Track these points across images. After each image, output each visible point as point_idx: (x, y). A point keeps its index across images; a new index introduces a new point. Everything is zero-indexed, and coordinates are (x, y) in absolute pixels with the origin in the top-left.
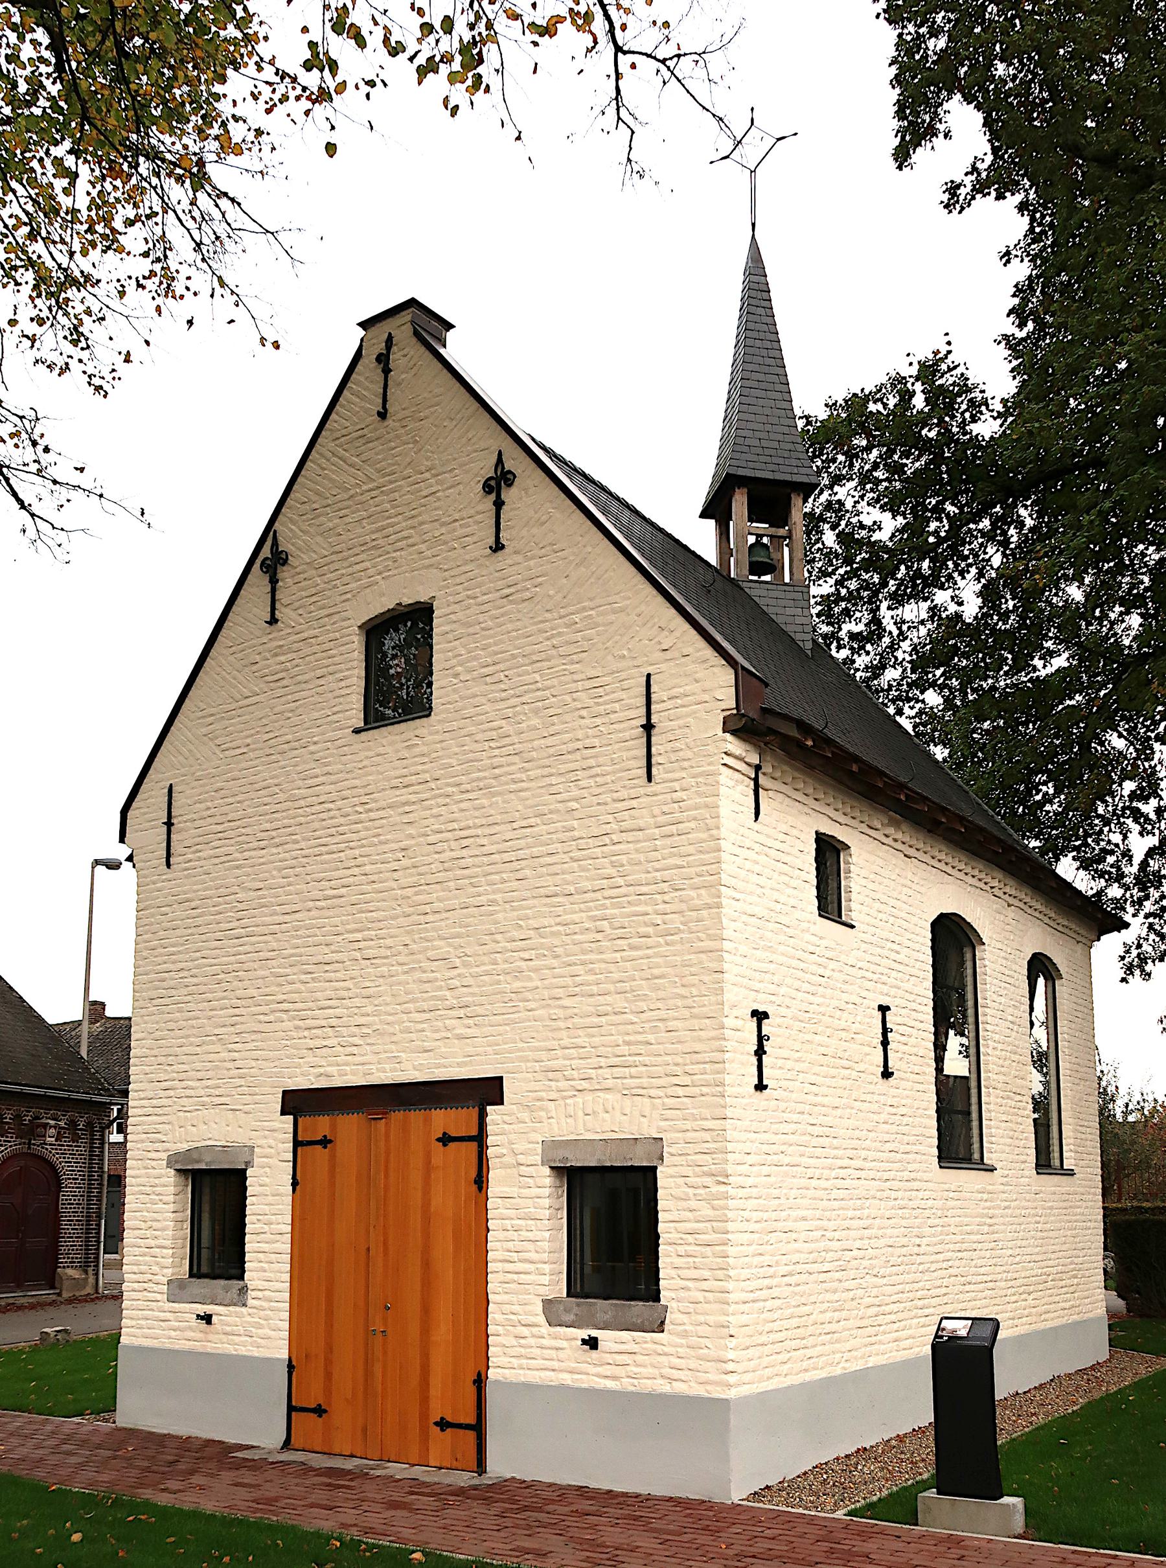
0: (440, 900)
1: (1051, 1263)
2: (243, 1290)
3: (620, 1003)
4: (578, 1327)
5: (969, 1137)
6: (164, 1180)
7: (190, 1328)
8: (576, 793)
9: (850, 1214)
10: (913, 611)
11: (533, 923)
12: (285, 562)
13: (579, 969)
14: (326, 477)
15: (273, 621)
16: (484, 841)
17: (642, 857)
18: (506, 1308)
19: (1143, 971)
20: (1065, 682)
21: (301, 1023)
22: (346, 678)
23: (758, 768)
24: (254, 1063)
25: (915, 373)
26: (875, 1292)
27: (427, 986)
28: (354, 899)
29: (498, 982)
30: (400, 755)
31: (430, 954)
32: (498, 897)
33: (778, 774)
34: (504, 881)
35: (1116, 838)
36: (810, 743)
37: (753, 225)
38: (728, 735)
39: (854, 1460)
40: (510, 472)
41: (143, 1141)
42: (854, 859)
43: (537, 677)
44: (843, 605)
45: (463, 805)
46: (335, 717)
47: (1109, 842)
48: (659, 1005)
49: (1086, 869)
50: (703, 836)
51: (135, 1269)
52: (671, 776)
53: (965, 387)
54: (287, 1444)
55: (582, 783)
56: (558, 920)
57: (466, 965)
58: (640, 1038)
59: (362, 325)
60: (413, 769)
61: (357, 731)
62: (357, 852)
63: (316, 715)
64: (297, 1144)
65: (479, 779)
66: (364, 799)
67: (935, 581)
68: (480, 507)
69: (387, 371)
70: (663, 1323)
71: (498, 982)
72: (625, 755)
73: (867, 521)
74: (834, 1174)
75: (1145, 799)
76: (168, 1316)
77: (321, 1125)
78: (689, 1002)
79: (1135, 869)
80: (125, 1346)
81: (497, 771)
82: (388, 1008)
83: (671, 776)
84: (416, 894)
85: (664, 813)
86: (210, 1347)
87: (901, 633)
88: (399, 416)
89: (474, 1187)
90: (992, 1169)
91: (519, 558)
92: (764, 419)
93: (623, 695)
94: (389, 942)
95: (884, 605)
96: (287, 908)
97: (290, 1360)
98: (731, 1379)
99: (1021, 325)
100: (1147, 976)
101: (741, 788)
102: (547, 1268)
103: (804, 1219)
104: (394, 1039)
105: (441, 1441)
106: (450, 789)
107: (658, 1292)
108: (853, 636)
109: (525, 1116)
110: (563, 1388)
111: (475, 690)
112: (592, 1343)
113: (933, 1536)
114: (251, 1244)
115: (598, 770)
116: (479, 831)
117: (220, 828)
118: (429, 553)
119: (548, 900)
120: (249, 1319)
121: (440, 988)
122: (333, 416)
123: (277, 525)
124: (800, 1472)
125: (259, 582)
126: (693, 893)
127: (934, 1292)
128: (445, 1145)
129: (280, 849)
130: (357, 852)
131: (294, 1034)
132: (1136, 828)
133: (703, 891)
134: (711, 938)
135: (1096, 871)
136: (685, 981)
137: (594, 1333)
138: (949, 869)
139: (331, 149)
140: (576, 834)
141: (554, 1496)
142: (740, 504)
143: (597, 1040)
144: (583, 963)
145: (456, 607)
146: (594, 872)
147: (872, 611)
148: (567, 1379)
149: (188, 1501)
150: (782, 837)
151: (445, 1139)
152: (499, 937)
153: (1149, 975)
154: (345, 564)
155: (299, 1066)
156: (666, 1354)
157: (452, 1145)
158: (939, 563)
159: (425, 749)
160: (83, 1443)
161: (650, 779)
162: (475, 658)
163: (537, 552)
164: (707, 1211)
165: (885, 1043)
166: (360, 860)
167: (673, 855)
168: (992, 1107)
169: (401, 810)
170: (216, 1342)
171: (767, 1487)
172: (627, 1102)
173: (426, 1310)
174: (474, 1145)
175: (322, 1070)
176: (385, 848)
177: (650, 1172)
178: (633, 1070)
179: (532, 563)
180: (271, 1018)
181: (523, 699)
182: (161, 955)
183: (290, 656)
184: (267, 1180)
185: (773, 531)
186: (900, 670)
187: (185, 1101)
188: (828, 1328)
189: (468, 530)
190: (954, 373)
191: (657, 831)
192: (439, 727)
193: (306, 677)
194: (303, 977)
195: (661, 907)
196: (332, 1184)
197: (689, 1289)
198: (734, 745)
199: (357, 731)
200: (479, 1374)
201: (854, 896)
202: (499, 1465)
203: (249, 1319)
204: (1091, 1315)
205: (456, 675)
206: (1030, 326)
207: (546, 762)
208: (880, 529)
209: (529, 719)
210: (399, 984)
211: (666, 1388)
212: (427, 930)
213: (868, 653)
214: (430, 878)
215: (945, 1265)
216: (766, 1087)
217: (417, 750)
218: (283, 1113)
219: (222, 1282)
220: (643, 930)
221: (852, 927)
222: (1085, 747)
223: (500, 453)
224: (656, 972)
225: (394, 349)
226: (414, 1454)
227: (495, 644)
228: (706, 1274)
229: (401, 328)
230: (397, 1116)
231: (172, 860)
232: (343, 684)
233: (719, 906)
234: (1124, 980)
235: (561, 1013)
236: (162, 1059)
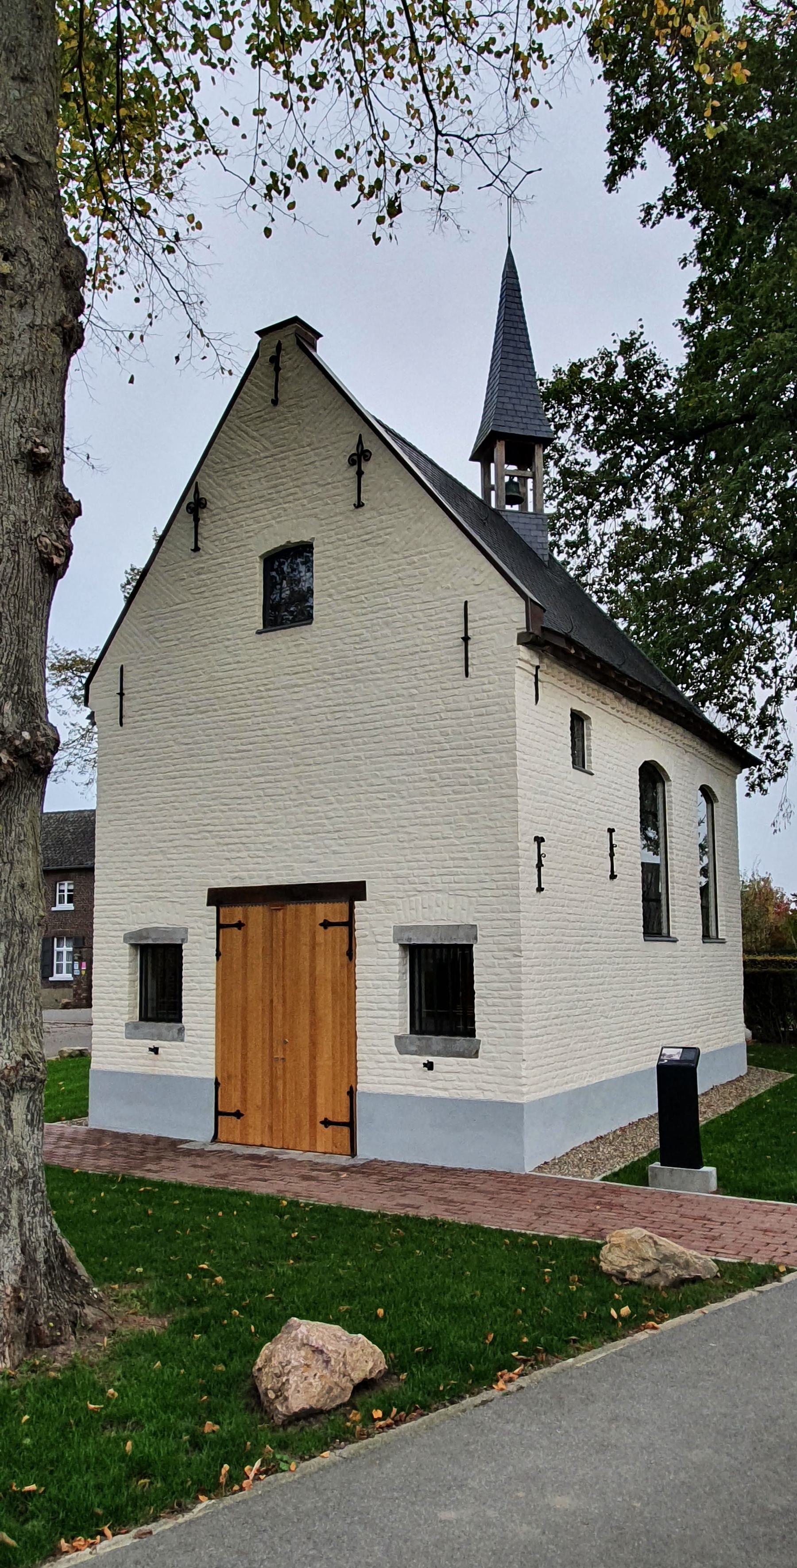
0: (320, 755)
1: (711, 1006)
2: (181, 1031)
3: (447, 830)
4: (420, 1055)
5: (660, 918)
6: (122, 951)
7: (143, 1057)
8: (416, 683)
9: (592, 974)
10: (612, 525)
11: (387, 773)
12: (205, 506)
13: (418, 807)
14: (233, 445)
15: (196, 549)
16: (351, 715)
17: (462, 730)
18: (370, 1042)
19: (761, 788)
20: (713, 574)
21: (221, 841)
22: (251, 593)
23: (537, 668)
24: (187, 869)
25: (618, 349)
26: (606, 1028)
27: (311, 816)
28: (259, 752)
29: (362, 815)
30: (290, 651)
31: (314, 793)
32: (361, 754)
33: (550, 671)
34: (365, 743)
35: (745, 689)
36: (573, 651)
37: (509, 238)
38: (521, 647)
39: (596, 1145)
40: (368, 451)
41: (105, 923)
42: (593, 727)
43: (388, 599)
44: (562, 520)
45: (337, 689)
46: (242, 622)
47: (740, 693)
48: (474, 833)
49: (723, 712)
50: (504, 716)
51: (101, 1015)
52: (482, 673)
53: (652, 361)
54: (215, 1139)
55: (420, 676)
56: (404, 772)
57: (339, 802)
58: (461, 855)
59: (258, 333)
60: (300, 662)
61: (259, 633)
62: (260, 719)
63: (230, 619)
64: (220, 926)
65: (347, 670)
66: (265, 681)
67: (625, 503)
68: (346, 475)
69: (277, 369)
70: (477, 1052)
71: (362, 815)
72: (449, 657)
73: (581, 460)
74: (582, 947)
75: (765, 661)
76: (127, 1049)
77: (237, 913)
78: (494, 831)
79: (757, 712)
80: (97, 1071)
81: (360, 665)
82: (283, 831)
83: (482, 673)
84: (303, 750)
85: (477, 700)
86: (157, 1071)
87: (603, 543)
88: (287, 404)
89: (346, 958)
90: (675, 941)
91: (375, 513)
92: (516, 389)
93: (448, 615)
94: (284, 784)
95: (592, 520)
96: (210, 758)
97: (216, 1079)
98: (525, 1089)
99: (691, 312)
100: (764, 792)
101: (527, 682)
102: (397, 1014)
103: (565, 979)
104: (289, 853)
105: (325, 1135)
106: (327, 677)
107: (474, 1030)
108: (567, 543)
109: (381, 908)
110: (409, 1097)
111: (344, 607)
112: (429, 1066)
113: (660, 1193)
114: (186, 998)
115: (431, 668)
116: (347, 708)
117: (159, 698)
118: (309, 506)
119: (396, 758)
120: (185, 1050)
121: (320, 818)
122: (238, 400)
123: (197, 479)
124: (563, 1153)
125: (186, 519)
126: (497, 756)
127: (640, 1028)
128: (325, 928)
129: (203, 715)
130: (260, 719)
131: (215, 848)
132: (759, 682)
133: (503, 754)
134: (509, 787)
135: (730, 714)
136: (491, 817)
137: (431, 1059)
138: (649, 729)
139: (268, 232)
140: (416, 711)
141: (407, 1170)
142: (500, 451)
143: (431, 857)
144: (422, 802)
145: (330, 547)
146: (428, 739)
147: (581, 525)
148: (412, 1090)
149: (169, 1177)
150: (551, 714)
151: (326, 924)
152: (362, 782)
153: (766, 791)
154: (249, 510)
155: (220, 871)
156: (480, 1073)
157: (331, 929)
158: (628, 490)
159: (308, 647)
160: (74, 1140)
161: (467, 675)
162: (345, 584)
163: (387, 510)
164: (508, 976)
165: (612, 855)
166: (262, 726)
167: (483, 729)
168: (675, 896)
169: (291, 690)
170: (161, 1067)
171: (546, 1163)
172: (452, 900)
173: (313, 1043)
174: (345, 930)
175: (236, 874)
176: (280, 717)
177: (467, 949)
178: (456, 878)
179: (383, 517)
180: (199, 836)
181: (378, 615)
182: (117, 789)
183: (210, 575)
184: (198, 952)
185: (521, 473)
186: (601, 570)
187: (136, 895)
188: (579, 1054)
189: (337, 491)
190: (644, 349)
191: (472, 711)
192: (318, 632)
193: (221, 592)
194: (222, 807)
195: (475, 765)
196: (245, 956)
197: (495, 1028)
198: (524, 652)
199: (259, 633)
200: (351, 1088)
201: (593, 752)
202: (365, 1152)
203: (185, 1050)
204: (735, 1042)
205: (330, 596)
206: (698, 312)
207: (395, 660)
208: (589, 464)
209: (382, 629)
210: (292, 814)
211: (481, 1097)
212: (310, 776)
213: (579, 557)
214: (312, 740)
215: (647, 1009)
216: (542, 889)
217: (302, 648)
218: (209, 904)
219: (166, 1024)
220: (462, 780)
221: (592, 774)
222: (726, 623)
223: (360, 436)
224: (472, 810)
225: (283, 353)
226: (306, 1145)
227: (358, 575)
228: (508, 1018)
229: (288, 340)
230: (291, 907)
231: (124, 721)
232: (248, 598)
233: (515, 765)
234: (748, 795)
235: (406, 837)
236: (118, 865)
